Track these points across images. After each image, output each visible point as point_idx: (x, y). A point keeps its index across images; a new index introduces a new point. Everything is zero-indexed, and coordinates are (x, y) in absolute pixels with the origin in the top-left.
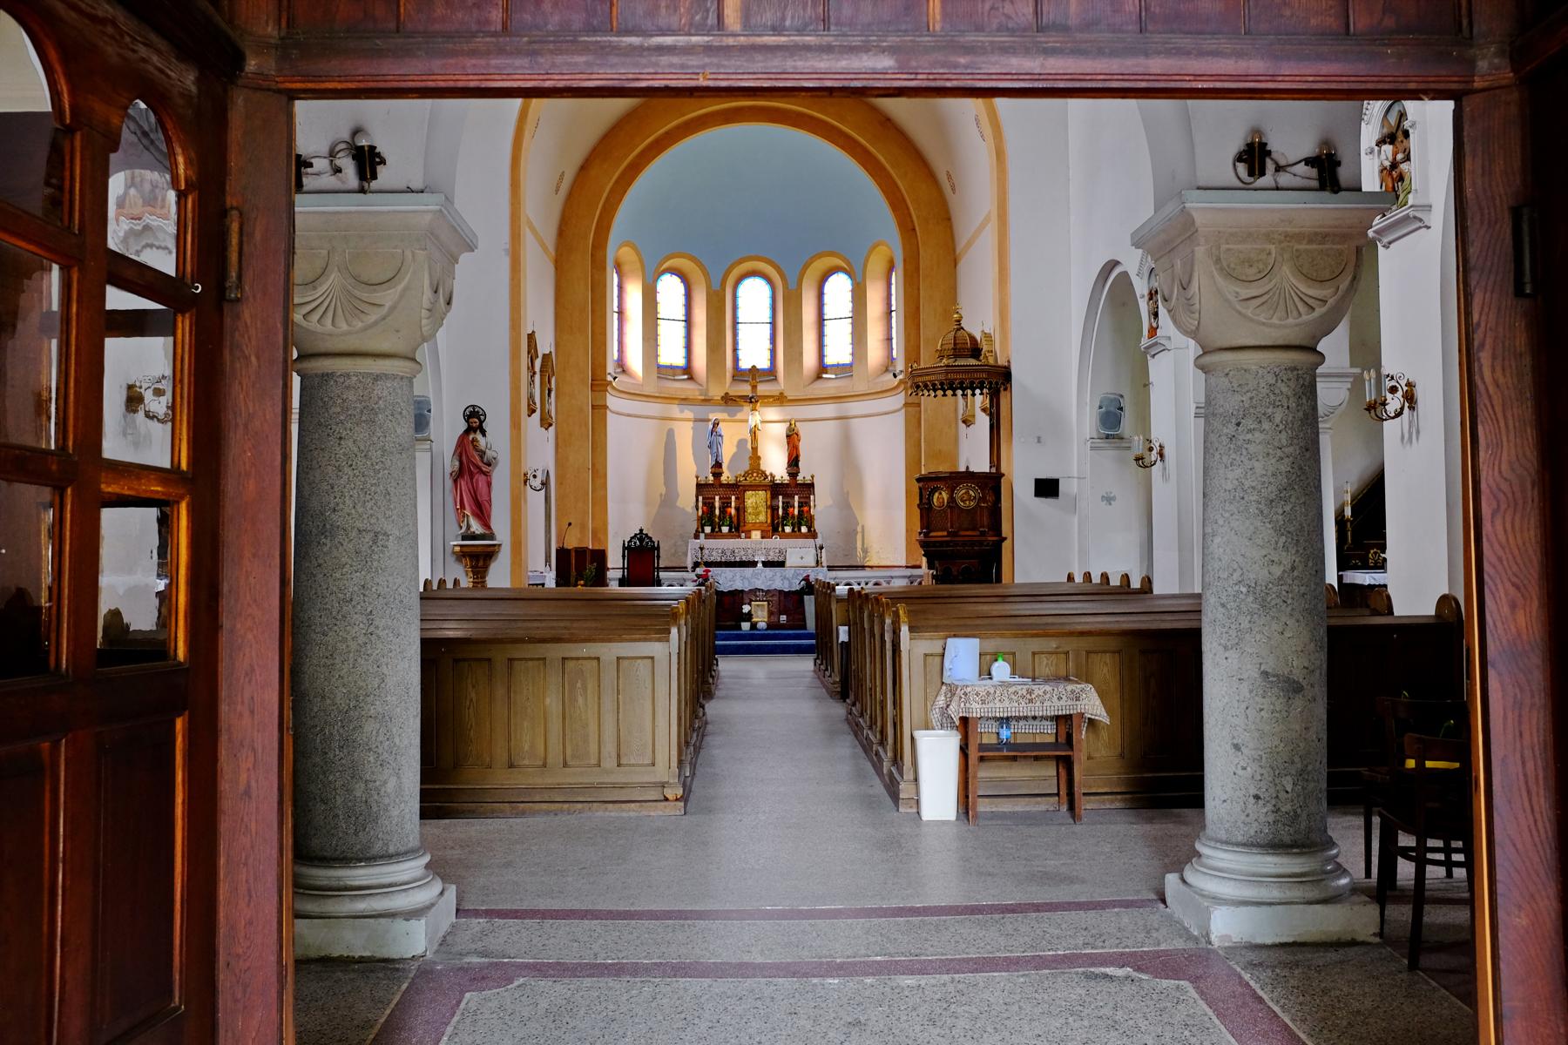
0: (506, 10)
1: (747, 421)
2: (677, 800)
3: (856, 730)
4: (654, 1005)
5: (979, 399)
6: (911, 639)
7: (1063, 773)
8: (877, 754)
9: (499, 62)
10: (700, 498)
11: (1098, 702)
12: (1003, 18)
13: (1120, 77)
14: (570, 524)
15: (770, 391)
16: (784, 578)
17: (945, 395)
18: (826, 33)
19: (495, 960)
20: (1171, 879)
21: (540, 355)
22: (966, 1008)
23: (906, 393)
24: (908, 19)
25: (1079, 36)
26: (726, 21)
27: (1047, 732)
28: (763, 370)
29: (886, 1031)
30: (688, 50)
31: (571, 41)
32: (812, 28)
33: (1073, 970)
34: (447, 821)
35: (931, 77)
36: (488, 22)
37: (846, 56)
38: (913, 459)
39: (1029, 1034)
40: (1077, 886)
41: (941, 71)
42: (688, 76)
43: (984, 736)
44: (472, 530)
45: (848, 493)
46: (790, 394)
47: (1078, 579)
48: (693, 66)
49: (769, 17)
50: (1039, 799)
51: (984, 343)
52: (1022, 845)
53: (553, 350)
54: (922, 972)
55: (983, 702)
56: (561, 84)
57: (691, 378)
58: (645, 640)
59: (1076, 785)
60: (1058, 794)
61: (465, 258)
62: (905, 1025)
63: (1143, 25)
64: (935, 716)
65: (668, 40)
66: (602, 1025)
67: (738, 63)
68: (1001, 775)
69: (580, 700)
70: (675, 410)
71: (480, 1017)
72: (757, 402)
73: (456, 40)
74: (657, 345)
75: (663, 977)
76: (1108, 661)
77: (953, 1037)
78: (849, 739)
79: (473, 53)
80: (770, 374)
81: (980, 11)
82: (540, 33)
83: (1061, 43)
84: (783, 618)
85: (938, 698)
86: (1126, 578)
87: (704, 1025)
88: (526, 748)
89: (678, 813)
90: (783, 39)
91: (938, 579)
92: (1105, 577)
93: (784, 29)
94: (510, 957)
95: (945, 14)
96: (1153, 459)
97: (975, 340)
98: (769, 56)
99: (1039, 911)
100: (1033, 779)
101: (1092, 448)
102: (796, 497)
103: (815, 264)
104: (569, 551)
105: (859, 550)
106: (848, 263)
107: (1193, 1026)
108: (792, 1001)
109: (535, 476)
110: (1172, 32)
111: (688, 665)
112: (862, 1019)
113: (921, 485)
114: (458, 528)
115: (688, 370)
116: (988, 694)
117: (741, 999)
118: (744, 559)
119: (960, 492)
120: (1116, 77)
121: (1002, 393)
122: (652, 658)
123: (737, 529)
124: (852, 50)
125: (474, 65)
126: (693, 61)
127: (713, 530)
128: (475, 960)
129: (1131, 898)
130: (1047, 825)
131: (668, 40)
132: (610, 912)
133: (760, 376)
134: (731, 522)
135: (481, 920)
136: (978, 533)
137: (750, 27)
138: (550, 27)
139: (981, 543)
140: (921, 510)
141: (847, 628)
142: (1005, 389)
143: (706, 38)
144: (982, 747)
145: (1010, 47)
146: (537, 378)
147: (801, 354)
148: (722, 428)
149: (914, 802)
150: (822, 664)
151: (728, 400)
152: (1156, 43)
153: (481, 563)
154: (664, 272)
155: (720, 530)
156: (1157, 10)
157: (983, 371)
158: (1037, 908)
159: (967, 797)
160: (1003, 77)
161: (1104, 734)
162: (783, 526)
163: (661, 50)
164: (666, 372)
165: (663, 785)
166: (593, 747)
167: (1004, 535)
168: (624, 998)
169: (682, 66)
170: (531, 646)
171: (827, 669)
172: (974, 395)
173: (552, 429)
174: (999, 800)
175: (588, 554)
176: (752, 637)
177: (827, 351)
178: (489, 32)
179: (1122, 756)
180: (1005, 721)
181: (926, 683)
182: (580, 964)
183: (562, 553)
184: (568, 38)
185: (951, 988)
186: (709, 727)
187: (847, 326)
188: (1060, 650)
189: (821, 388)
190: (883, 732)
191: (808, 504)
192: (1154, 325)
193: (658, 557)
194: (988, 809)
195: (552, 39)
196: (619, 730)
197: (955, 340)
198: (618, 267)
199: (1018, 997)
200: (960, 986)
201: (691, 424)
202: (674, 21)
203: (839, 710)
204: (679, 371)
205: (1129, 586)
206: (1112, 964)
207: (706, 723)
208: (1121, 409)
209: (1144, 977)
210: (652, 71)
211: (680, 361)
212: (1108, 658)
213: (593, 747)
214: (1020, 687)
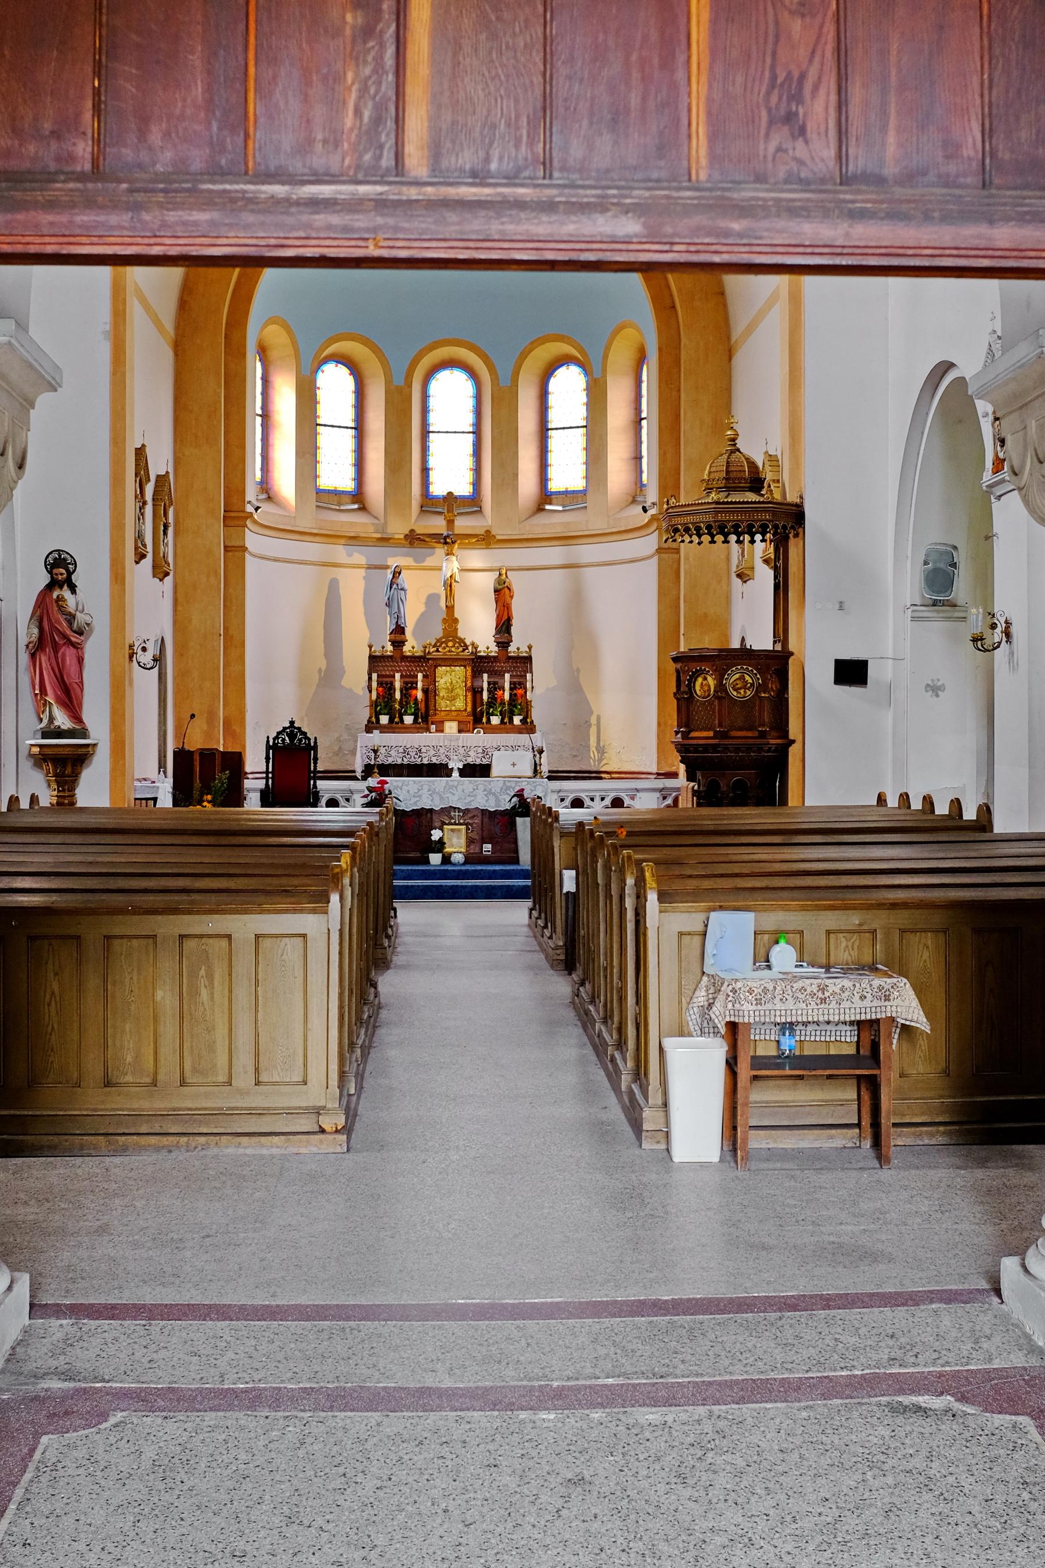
0: (97, 141)
1: (440, 569)
2: (337, 1131)
3: (586, 1021)
4: (301, 1453)
5: (759, 547)
6: (661, 912)
7: (866, 1096)
8: (613, 1060)
9: (85, 218)
10: (375, 676)
11: (915, 1003)
12: (794, 166)
13: (955, 252)
14: (193, 716)
15: (473, 527)
16: (489, 793)
17: (713, 542)
18: (546, 182)
19: (83, 1385)
20: (1009, 1265)
21: (153, 478)
22: (728, 1457)
23: (660, 536)
24: (662, 163)
25: (899, 192)
26: (407, 161)
27: (845, 1042)
28: (463, 498)
29: (618, 1493)
30: (355, 205)
31: (188, 190)
32: (526, 173)
33: (874, 1400)
34: (19, 1161)
35: (692, 248)
36: (71, 158)
37: (574, 218)
38: (668, 631)
39: (813, 1497)
40: (882, 1266)
41: (706, 240)
42: (353, 243)
43: (760, 1045)
44: (56, 723)
45: (578, 670)
46: (499, 533)
47: (892, 802)
48: (359, 230)
49: (467, 159)
50: (833, 1132)
51: (768, 468)
52: (807, 1201)
53: (171, 470)
54: (670, 1402)
55: (759, 1002)
56: (174, 251)
57: (363, 508)
58: (295, 911)
59: (883, 1115)
60: (858, 1125)
61: (44, 400)
62: (645, 1484)
63: (987, 176)
64: (693, 1018)
65: (325, 190)
66: (230, 1484)
67: (424, 226)
68: (782, 1098)
69: (204, 994)
70: (340, 553)
71: (61, 1473)
72: (453, 543)
73: (28, 185)
74: (317, 462)
75: (315, 1410)
76: (929, 942)
77: (710, 1502)
78: (576, 1032)
79: (51, 205)
80: (473, 503)
81: (761, 153)
82: (145, 176)
83: (874, 202)
84: (487, 847)
85: (697, 993)
86: (956, 805)
87: (371, 1484)
88: (129, 1059)
89: (338, 1149)
90: (484, 192)
91: (706, 797)
92: (928, 802)
93: (489, 174)
94: (103, 1381)
95: (714, 158)
96: (997, 639)
97: (757, 467)
98: (468, 216)
99: (828, 1307)
100: (827, 1103)
101: (914, 619)
102: (507, 676)
103: (536, 351)
104: (191, 754)
105: (593, 749)
106: (581, 351)
107: (1035, 1484)
108: (491, 1447)
109: (144, 649)
110: (1026, 186)
111: (355, 938)
112: (587, 1474)
113: (679, 666)
114: (36, 720)
115: (358, 496)
116: (765, 990)
117: (421, 1443)
118: (434, 760)
119: (733, 677)
120: (948, 252)
121: (792, 541)
122: (304, 936)
123: (425, 719)
124: (583, 208)
125: (52, 224)
126: (360, 221)
127: (391, 721)
128: (55, 1384)
129: (954, 1287)
130: (843, 1169)
131: (325, 190)
132: (242, 1308)
133: (459, 506)
134: (417, 709)
135: (64, 1322)
136: (756, 734)
137: (441, 171)
138: (159, 168)
139: (760, 749)
140: (678, 700)
141: (573, 873)
142: (796, 536)
143: (379, 189)
144: (758, 1062)
145: (802, 208)
146: (149, 509)
147: (516, 475)
148: (405, 578)
149: (661, 1135)
150: (539, 918)
151: (414, 539)
152: (1005, 204)
153: (69, 770)
154: (326, 360)
155: (402, 721)
156: (1007, 156)
157: (765, 510)
158: (827, 1302)
159: (735, 1128)
160: (791, 250)
161: (923, 1043)
162: (489, 715)
163: (315, 204)
164: (329, 498)
165: (318, 1111)
166: (222, 1060)
167: (791, 737)
168: (261, 1443)
169: (346, 229)
170: (136, 918)
171: (546, 927)
172: (752, 542)
173: (169, 580)
174: (779, 1132)
175: (218, 757)
176: (445, 875)
177: (552, 472)
178: (73, 173)
179: (946, 1072)
180: (788, 1027)
181: (680, 972)
182: (200, 1391)
183: (182, 757)
184: (184, 185)
185: (708, 1427)
186: (384, 1014)
187: (578, 438)
188: (865, 927)
189: (544, 524)
190: (621, 1030)
191: (522, 685)
192: (1001, 455)
193: (316, 759)
194: (764, 1146)
195: (161, 186)
196: (257, 1035)
197: (727, 467)
198: (263, 351)
199: (798, 1441)
200: (722, 1424)
201: (362, 572)
202: (334, 162)
203: (562, 986)
204: (347, 499)
205: (961, 816)
206: (927, 1391)
207: (380, 1007)
208: (954, 565)
209: (970, 1409)
210: (302, 234)
211: (346, 482)
212: (929, 939)
213: (222, 1060)
214: (808, 981)
